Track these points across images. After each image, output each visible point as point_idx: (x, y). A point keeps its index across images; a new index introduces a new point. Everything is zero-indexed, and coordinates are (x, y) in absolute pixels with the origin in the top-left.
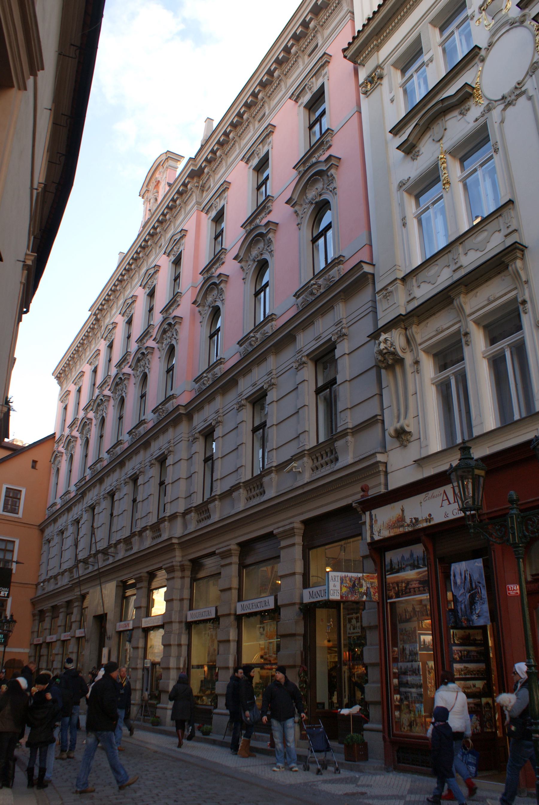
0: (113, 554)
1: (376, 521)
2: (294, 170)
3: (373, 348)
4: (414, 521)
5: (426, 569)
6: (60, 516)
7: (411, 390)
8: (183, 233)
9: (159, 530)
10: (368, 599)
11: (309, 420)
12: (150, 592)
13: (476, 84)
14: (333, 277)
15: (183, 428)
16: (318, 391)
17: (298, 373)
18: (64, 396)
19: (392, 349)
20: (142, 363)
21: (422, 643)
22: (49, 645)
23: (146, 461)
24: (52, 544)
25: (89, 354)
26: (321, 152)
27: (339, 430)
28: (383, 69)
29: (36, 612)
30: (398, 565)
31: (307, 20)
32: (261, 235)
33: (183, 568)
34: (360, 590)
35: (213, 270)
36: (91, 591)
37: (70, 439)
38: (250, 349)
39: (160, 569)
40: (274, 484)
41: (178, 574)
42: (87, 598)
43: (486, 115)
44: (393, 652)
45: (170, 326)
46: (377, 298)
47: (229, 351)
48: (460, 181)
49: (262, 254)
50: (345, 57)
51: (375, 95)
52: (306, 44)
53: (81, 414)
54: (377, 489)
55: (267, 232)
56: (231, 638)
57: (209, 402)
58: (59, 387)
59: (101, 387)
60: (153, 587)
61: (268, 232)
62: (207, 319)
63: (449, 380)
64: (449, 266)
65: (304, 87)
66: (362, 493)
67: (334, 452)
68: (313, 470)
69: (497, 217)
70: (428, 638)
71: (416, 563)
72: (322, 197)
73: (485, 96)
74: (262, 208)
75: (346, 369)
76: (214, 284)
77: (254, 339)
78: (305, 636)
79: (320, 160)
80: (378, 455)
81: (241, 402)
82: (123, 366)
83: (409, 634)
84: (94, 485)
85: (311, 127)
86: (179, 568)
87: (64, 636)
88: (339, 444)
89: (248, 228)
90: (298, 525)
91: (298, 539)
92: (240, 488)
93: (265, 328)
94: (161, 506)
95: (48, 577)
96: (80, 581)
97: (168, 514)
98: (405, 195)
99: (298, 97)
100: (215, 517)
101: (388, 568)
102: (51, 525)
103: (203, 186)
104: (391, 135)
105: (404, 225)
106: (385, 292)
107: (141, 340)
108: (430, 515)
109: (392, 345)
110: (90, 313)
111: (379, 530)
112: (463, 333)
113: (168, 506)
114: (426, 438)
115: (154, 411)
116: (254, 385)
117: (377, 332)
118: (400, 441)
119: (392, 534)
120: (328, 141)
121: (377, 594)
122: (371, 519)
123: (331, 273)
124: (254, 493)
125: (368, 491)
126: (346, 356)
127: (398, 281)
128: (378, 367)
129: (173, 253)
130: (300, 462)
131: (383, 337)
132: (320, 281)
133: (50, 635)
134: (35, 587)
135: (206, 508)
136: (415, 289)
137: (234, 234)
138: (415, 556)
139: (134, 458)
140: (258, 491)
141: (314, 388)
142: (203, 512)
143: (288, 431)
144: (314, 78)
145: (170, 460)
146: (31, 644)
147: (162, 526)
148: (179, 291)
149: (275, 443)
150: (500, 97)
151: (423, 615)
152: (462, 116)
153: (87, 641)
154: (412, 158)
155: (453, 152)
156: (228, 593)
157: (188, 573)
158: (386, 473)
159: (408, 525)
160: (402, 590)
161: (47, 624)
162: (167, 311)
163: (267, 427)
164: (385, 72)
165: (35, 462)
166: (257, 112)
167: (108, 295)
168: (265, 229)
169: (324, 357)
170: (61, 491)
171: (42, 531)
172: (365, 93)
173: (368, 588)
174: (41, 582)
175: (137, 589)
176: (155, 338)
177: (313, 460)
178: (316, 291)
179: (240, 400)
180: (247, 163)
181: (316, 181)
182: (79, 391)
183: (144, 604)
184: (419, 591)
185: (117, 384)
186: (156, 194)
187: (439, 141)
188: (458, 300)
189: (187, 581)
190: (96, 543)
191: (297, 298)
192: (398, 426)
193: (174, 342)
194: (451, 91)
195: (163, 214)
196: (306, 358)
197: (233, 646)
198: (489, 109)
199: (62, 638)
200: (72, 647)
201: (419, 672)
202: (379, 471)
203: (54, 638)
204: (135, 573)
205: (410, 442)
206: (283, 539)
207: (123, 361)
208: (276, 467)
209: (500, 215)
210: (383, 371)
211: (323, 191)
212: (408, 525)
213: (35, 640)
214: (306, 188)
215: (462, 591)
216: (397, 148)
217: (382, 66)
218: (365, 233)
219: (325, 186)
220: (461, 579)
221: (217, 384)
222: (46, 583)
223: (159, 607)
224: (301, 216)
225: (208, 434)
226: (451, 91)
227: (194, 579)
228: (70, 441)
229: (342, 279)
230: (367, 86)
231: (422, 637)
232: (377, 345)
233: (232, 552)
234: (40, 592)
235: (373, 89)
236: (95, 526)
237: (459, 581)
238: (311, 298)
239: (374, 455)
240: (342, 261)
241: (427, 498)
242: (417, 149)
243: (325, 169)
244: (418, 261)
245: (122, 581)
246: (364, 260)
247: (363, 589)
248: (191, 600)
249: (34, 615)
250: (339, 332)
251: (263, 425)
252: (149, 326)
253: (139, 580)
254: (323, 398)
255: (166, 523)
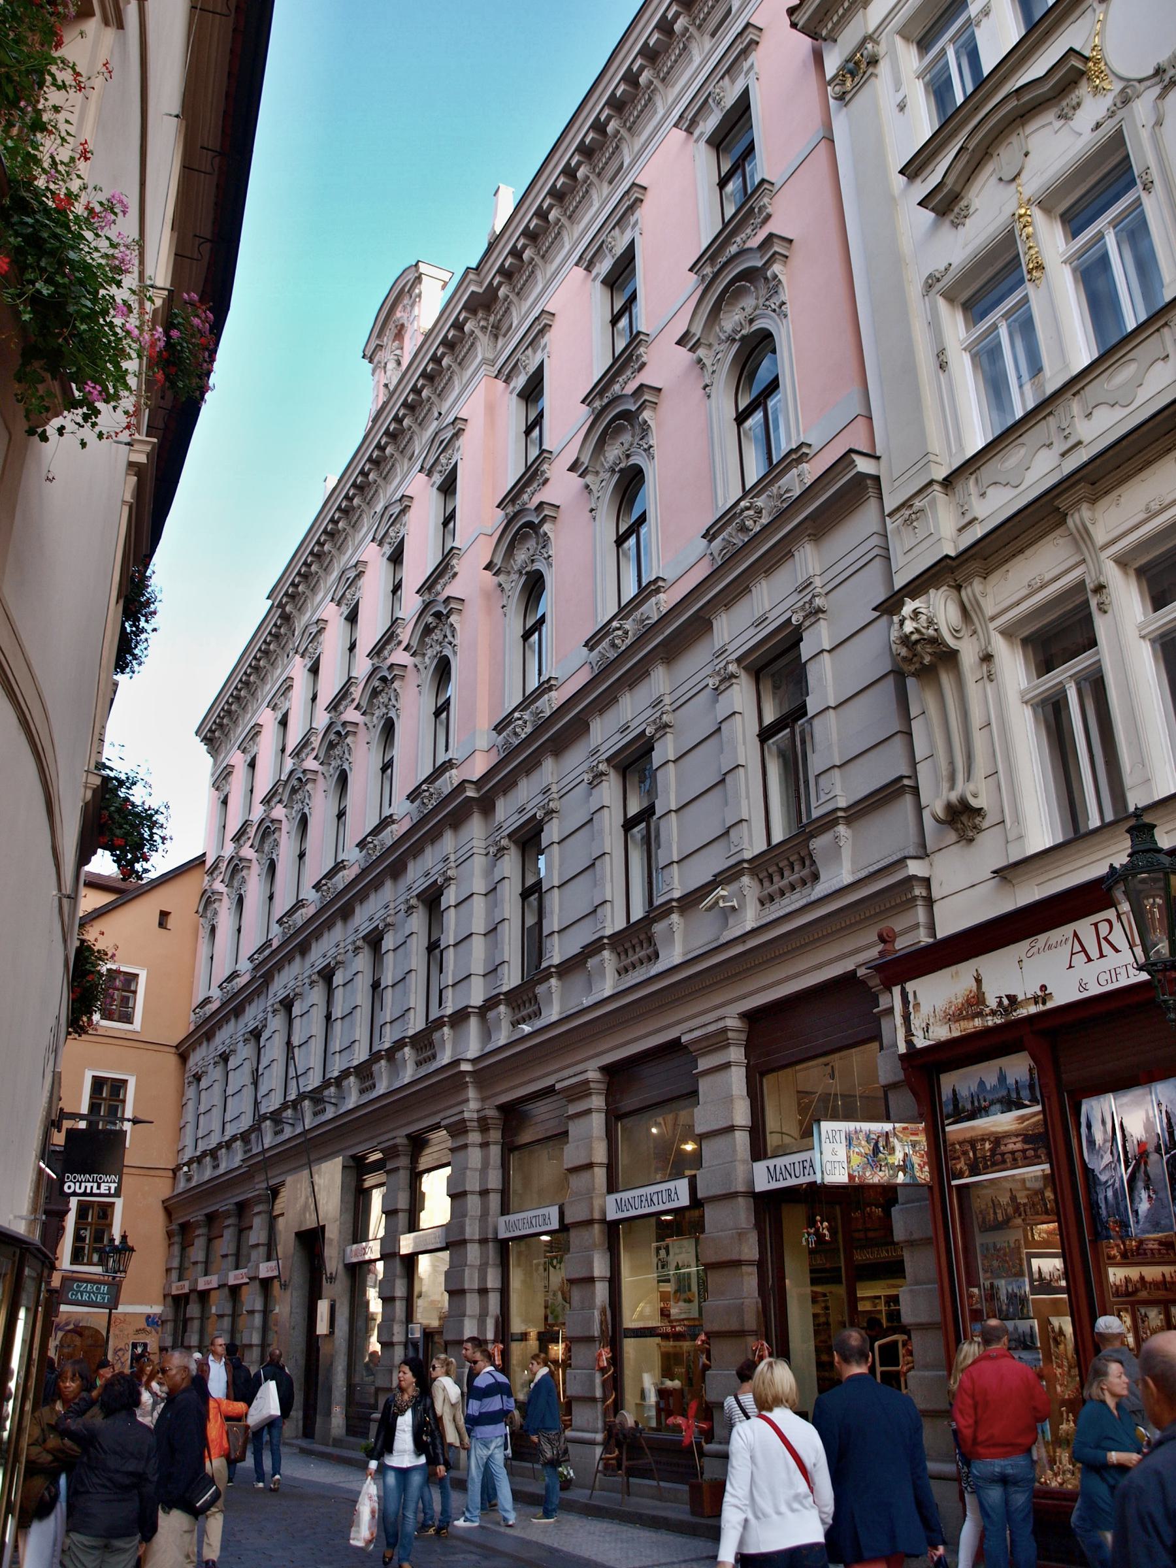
0: (333, 1101)
1: (917, 1005)
2: (692, 274)
3: (887, 633)
4: (1006, 1002)
5: (1038, 1108)
6: (219, 1025)
7: (976, 717)
8: (458, 427)
9: (431, 1044)
10: (908, 1181)
11: (748, 797)
12: (416, 1177)
13: (1093, 49)
14: (787, 491)
15: (475, 829)
16: (765, 735)
17: (594, 791)
18: (222, 777)
19: (931, 632)
20: (382, 698)
21: (1036, 1276)
22: (204, 1296)
23: (398, 902)
24: (204, 1084)
25: (269, 689)
26: (749, 231)
27: (815, 814)
28: (878, 44)
29: (174, 1227)
30: (973, 1103)
31: (670, 16)
32: (626, 415)
33: (483, 1125)
34: (890, 1161)
35: (525, 497)
36: (289, 1179)
37: (237, 865)
38: (612, 655)
39: (436, 1127)
40: (678, 937)
41: (474, 1137)
42: (282, 1195)
43: (1120, 114)
44: (971, 1296)
45: (437, 617)
46: (890, 527)
47: (567, 662)
48: (1065, 262)
49: (628, 456)
50: (794, 25)
51: (861, 101)
52: (706, 10)
53: (258, 812)
54: (913, 936)
55: (765, 264)
56: (596, 1273)
57: (528, 773)
58: (211, 760)
59: (297, 753)
60: (422, 1167)
61: (641, 408)
62: (515, 600)
63: (1064, 692)
64: (1050, 445)
65: (706, 101)
66: (881, 947)
67: (807, 863)
68: (762, 903)
69: (1158, 330)
70: (1050, 1265)
71: (1014, 1095)
72: (756, 326)
73: (1113, 73)
74: (626, 360)
75: (826, 681)
76: (529, 524)
77: (620, 633)
78: (761, 1264)
79: (748, 245)
80: (909, 862)
81: (597, 766)
82: (341, 708)
83: (1005, 1255)
84: (289, 959)
85: (615, 321)
86: (475, 1124)
87: (234, 1278)
88: (818, 844)
89: (597, 404)
90: (732, 1023)
91: (736, 1054)
92: (602, 948)
93: (537, 704)
94: (434, 993)
95: (198, 1153)
96: (265, 1159)
97: (449, 1011)
98: (942, 303)
99: (694, 122)
100: (553, 1013)
101: (948, 1109)
102: (200, 1045)
103: (496, 327)
104: (903, 179)
105: (943, 366)
106: (908, 512)
107: (378, 653)
108: (1043, 988)
109: (930, 622)
110: (270, 602)
111: (924, 1025)
112: (1090, 585)
113: (449, 994)
114: (1017, 820)
115: (413, 796)
116: (624, 729)
117: (895, 598)
118: (956, 830)
119: (956, 1034)
120: (764, 206)
121: (926, 1168)
122: (905, 1002)
123: (784, 482)
124: (633, 958)
125: (893, 941)
126: (825, 654)
127: (936, 487)
128: (898, 675)
129: (439, 468)
130: (734, 887)
131: (909, 607)
132: (760, 502)
133: (206, 1275)
134: (170, 1174)
135: (531, 995)
136: (974, 499)
137: (567, 418)
138: (1010, 1081)
139: (326, 935)
140: (642, 954)
141: (756, 729)
142: (524, 1003)
143: (705, 822)
144: (727, 78)
145: (450, 897)
146: (165, 1296)
147: (436, 1036)
148: (455, 545)
149: (836, 749)
150: (1151, 72)
151: (1037, 1213)
152: (1063, 122)
153: (284, 1286)
154: (952, 222)
155: (1045, 204)
156: (585, 1176)
157: (495, 1135)
158: (929, 902)
159: (993, 1013)
160: (984, 1157)
161: (197, 1253)
162: (430, 589)
163: (655, 817)
164: (882, 49)
165: (164, 915)
166: (606, 163)
167: (305, 563)
168: (635, 403)
169: (778, 662)
170: (222, 971)
171: (183, 1057)
172: (841, 98)
173: (906, 1155)
174: (184, 1165)
175: (388, 1172)
176: (408, 645)
177: (761, 881)
178: (751, 522)
179: (595, 763)
180: (588, 269)
181: (739, 293)
182: (252, 765)
183: (403, 1202)
184: (1026, 1158)
185: (332, 745)
186: (398, 352)
187: (1014, 179)
188: (1076, 516)
189: (495, 1151)
190: (297, 1077)
191: (710, 541)
192: (954, 797)
193: (447, 652)
194: (1037, 68)
195: (416, 391)
196: (736, 665)
197: (601, 1292)
198: (1125, 100)
199: (231, 1282)
200: (252, 1299)
201: (1033, 1342)
202: (915, 898)
203: (213, 1281)
204: (382, 1138)
205: (981, 831)
206: (704, 1054)
207: (387, 642)
208: (678, 900)
209: (1051, 413)
210: (911, 682)
211: (758, 312)
212: (993, 1013)
213: (174, 1286)
214: (720, 309)
215: (1107, 1158)
216: (920, 204)
217: (875, 36)
218: (855, 390)
219: (761, 301)
220: (1105, 1131)
221: (543, 734)
222: (195, 1165)
223: (437, 1209)
224: (597, 495)
225: (528, 839)
226: (1037, 68)
227: (509, 1148)
228: (237, 867)
229: (665, 618)
230: (843, 82)
231: (1035, 1263)
232: (896, 626)
233: (592, 1085)
234: (182, 1185)
235: (858, 88)
236: (296, 1041)
237: (1099, 1137)
238: (740, 539)
239: (901, 862)
240: (807, 454)
241: (1035, 950)
242: (963, 204)
243: (760, 264)
244: (976, 441)
245: (353, 1157)
246: (856, 448)
247: (897, 1158)
248: (505, 1192)
249: (170, 1235)
250: (807, 606)
251: (647, 813)
252: (395, 622)
253: (391, 1153)
254: (774, 748)
255: (446, 1029)
